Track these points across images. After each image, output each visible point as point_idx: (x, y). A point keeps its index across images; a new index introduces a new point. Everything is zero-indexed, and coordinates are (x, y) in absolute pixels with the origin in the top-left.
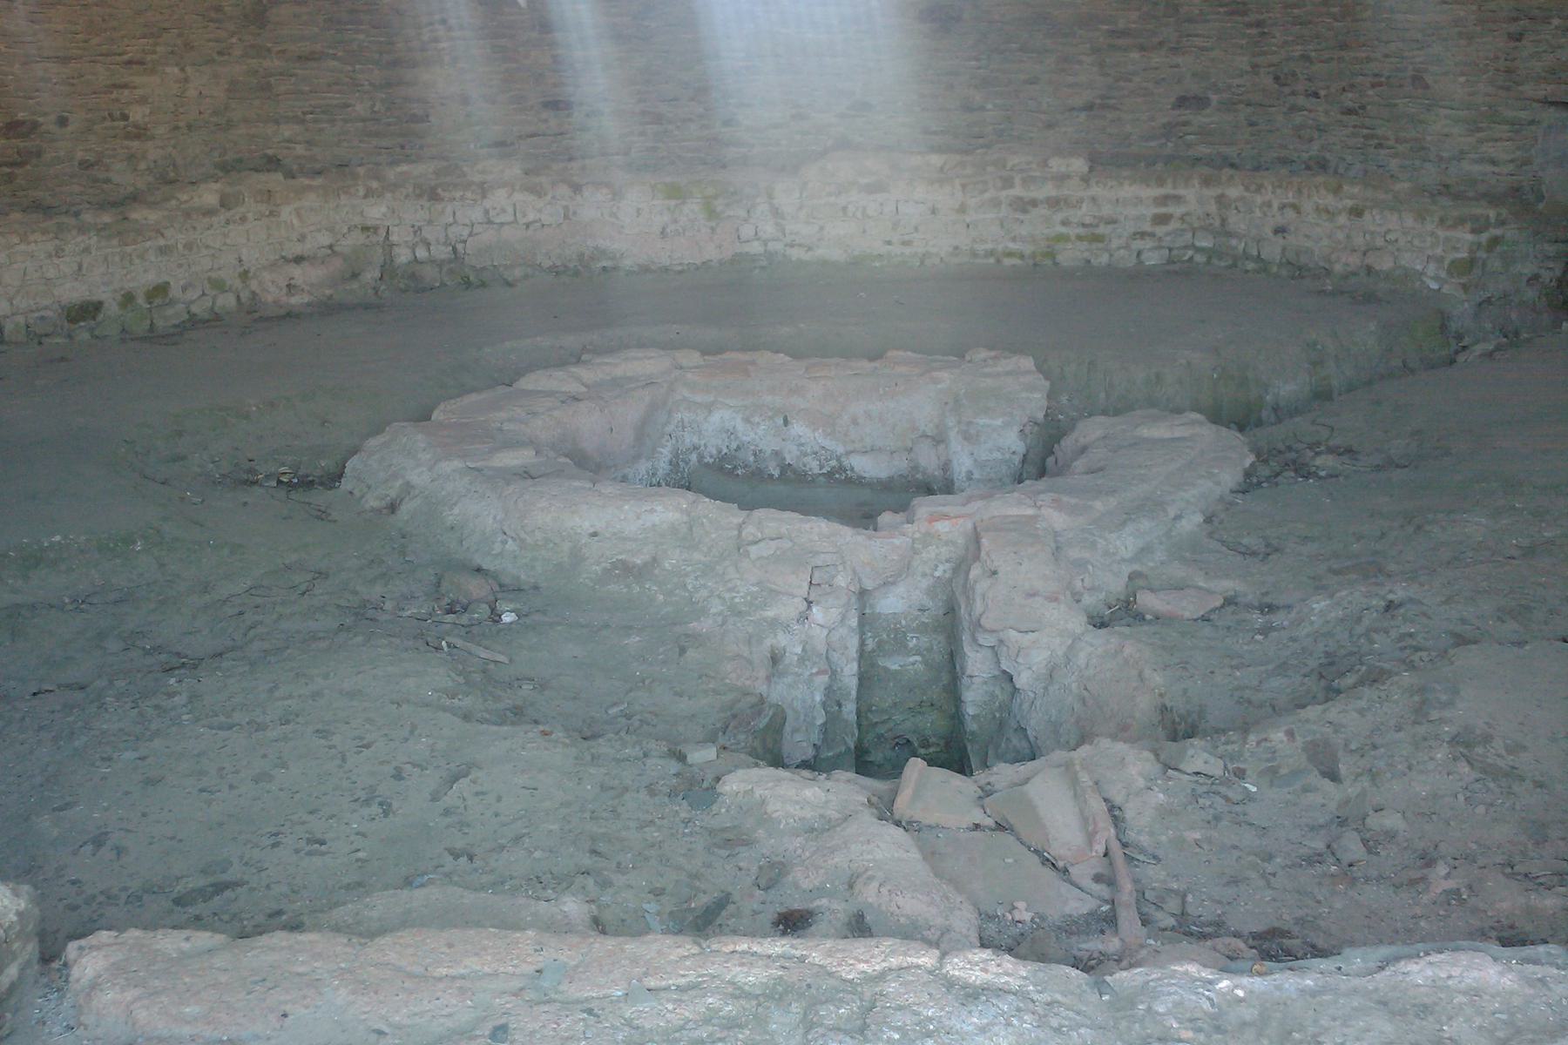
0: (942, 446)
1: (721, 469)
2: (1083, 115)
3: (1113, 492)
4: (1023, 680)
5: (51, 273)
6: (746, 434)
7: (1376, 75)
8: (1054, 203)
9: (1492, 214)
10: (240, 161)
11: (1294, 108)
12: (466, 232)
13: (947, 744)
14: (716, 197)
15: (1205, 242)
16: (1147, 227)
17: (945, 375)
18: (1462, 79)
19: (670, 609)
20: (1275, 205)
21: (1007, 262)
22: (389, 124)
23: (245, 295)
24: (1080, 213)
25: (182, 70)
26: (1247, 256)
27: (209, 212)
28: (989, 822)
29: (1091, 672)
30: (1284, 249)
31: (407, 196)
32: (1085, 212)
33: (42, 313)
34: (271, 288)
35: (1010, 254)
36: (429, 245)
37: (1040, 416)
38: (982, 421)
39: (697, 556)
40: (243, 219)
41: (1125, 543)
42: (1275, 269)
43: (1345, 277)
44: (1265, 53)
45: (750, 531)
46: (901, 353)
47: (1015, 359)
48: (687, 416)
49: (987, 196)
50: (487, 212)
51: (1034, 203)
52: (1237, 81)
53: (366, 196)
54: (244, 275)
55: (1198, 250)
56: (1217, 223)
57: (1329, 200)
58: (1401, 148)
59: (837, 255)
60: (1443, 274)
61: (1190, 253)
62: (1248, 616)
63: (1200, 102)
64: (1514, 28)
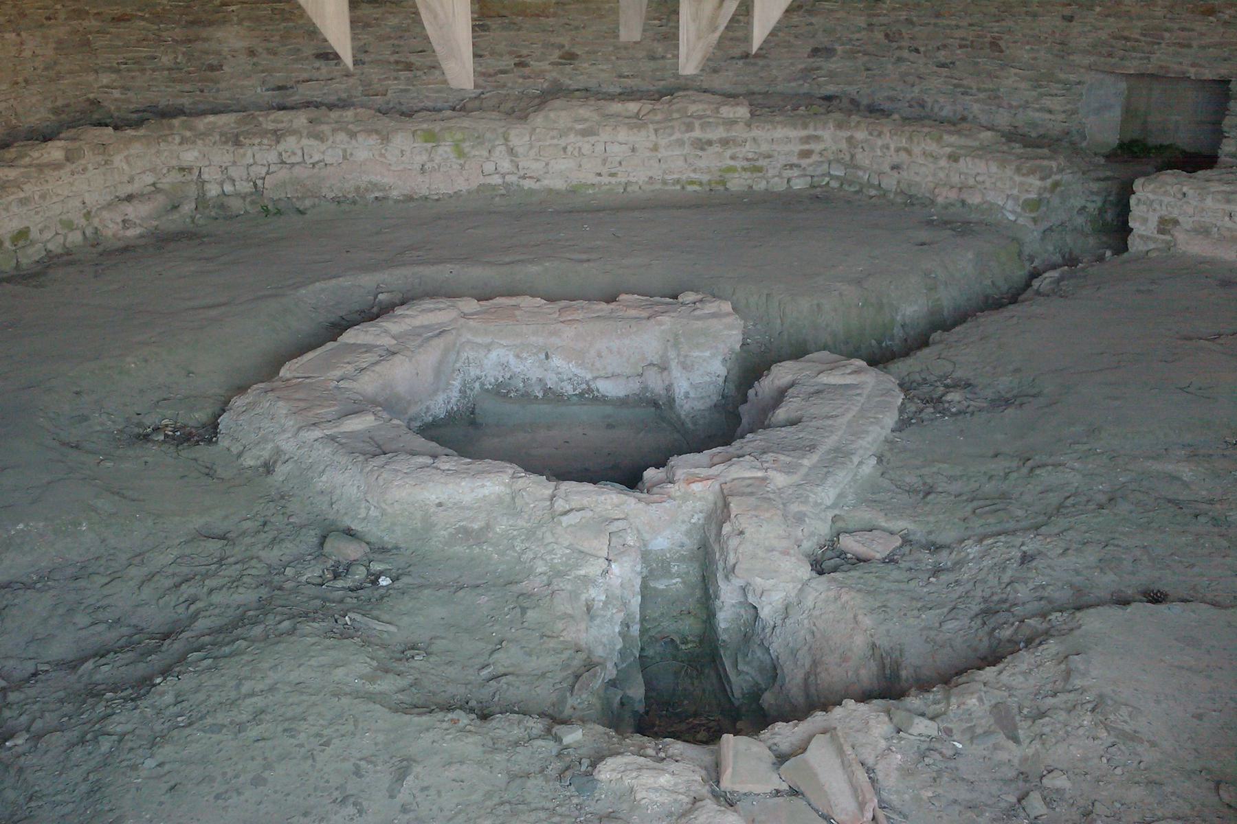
0: (666, 373)
1: (498, 393)
2: (741, 63)
4: (765, 613)
6: (517, 367)
7: (963, 39)
8: (725, 142)
9: (1054, 164)
11: (899, 59)
12: (264, 171)
13: (701, 642)
14: (464, 140)
15: (838, 172)
16: (795, 160)
18: (1028, 47)
19: (504, 567)
20: (892, 147)
21: (690, 188)
23: (89, 232)
24: (744, 150)
25: (19, 35)
27: (57, 166)
28: (784, 787)
29: (817, 613)
30: (899, 182)
31: (215, 143)
32: (748, 150)
34: (111, 226)
35: (692, 183)
37: (737, 347)
38: (696, 354)
39: (521, 523)
41: (827, 494)
42: (892, 196)
43: (945, 207)
45: (560, 505)
47: (716, 303)
48: (472, 354)
50: (280, 154)
51: (710, 143)
52: (856, 36)
53: (181, 144)
54: (88, 215)
55: (832, 177)
56: (848, 158)
57: (932, 147)
58: (982, 96)
59: (560, 184)
60: (1019, 210)
61: (827, 179)
62: (921, 556)
63: (829, 52)
64: (1067, 11)
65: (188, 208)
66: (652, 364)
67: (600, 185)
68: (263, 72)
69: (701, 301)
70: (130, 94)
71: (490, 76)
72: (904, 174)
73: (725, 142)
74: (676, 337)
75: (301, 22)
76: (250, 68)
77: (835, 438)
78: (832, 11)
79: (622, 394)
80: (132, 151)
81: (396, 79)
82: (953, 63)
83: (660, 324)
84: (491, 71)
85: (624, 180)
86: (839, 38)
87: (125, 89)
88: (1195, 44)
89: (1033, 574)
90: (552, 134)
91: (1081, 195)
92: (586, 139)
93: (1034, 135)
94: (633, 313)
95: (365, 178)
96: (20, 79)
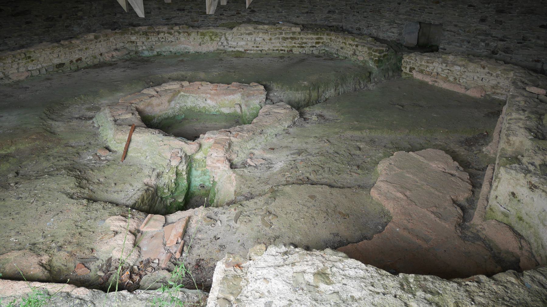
2: (305, 15)
5: (51, 57)
8: (292, 38)
11: (354, 15)
16: (314, 45)
32: (300, 41)
35: (282, 50)
40: (100, 41)
51: (287, 38)
57: (352, 42)
63: (334, 12)
67: (254, 50)
73: (292, 38)
84: (229, 15)
88: (433, 13)
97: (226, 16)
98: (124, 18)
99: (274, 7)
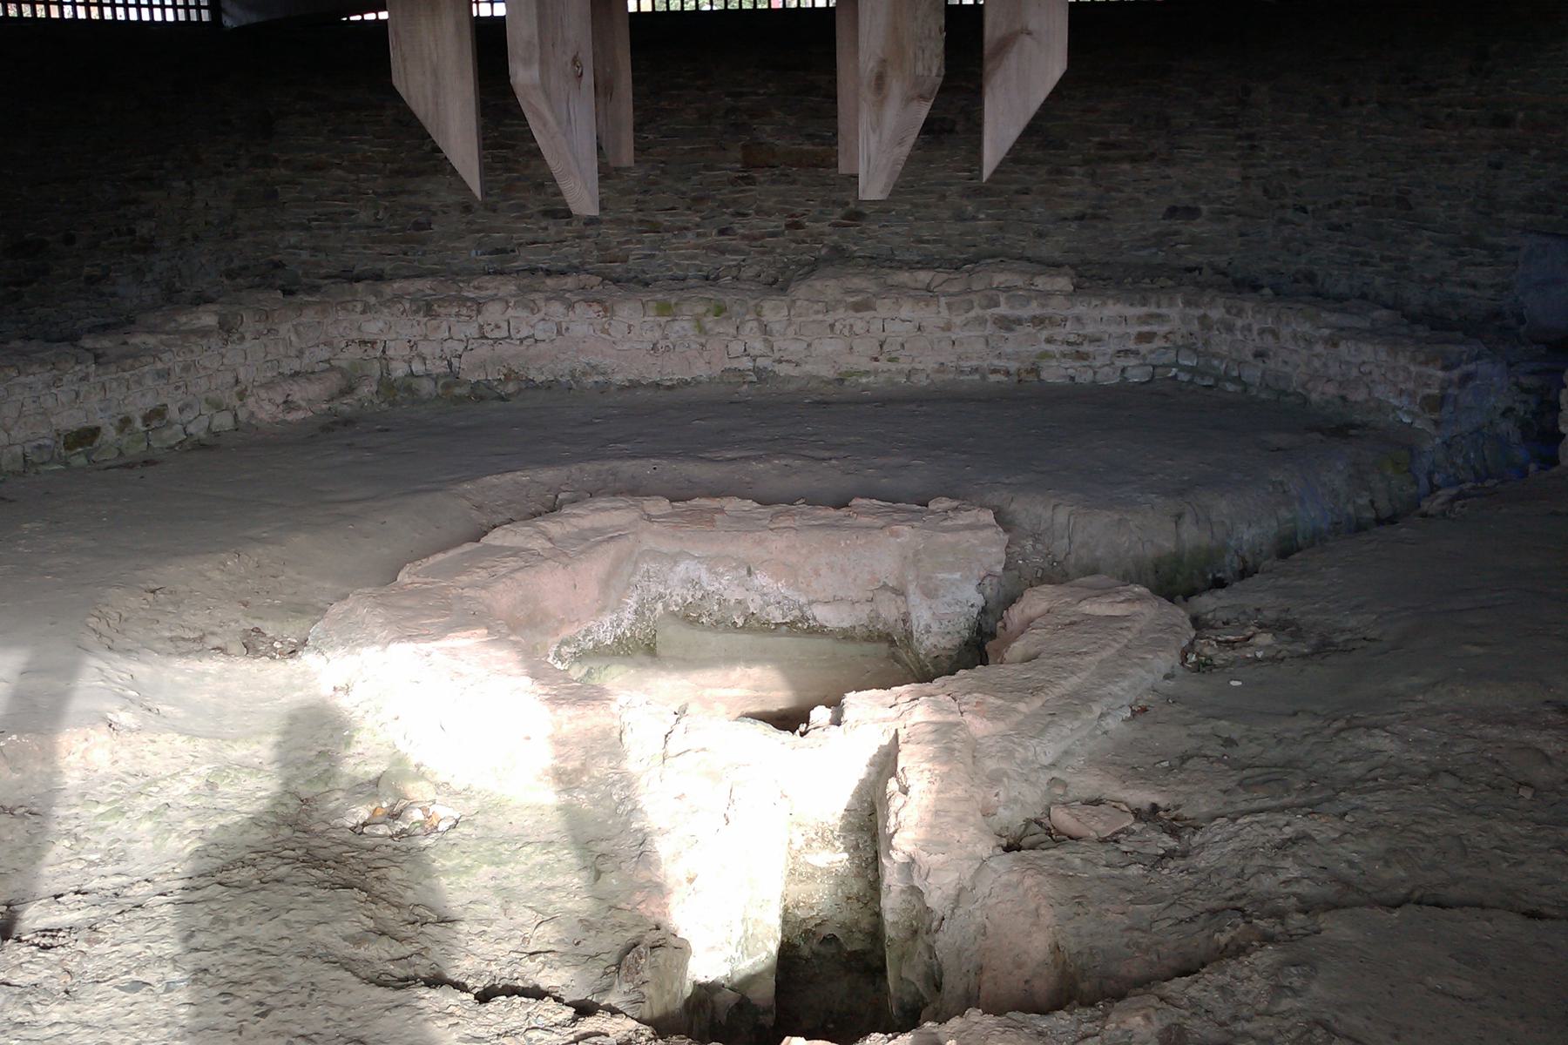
2: (1074, 225)
3: (1036, 690)
5: (50, 402)
8: (1038, 321)
10: (246, 268)
11: (1282, 221)
12: (460, 347)
15: (1189, 361)
16: (1131, 345)
17: (905, 529)
18: (1445, 203)
20: (1255, 327)
21: (993, 378)
22: (392, 231)
25: (189, 183)
26: (1227, 377)
27: (205, 333)
30: (1263, 374)
32: (1068, 331)
33: (41, 442)
34: (264, 409)
35: (995, 371)
36: (424, 359)
44: (1253, 166)
46: (865, 501)
49: (972, 314)
50: (481, 327)
51: (1019, 321)
52: (1226, 193)
55: (1183, 368)
57: (1306, 327)
58: (1386, 267)
59: (827, 372)
60: (1416, 409)
63: (1191, 213)
65: (366, 390)
66: (885, 587)
67: (876, 372)
68: (479, 231)
69: (956, 509)
70: (322, 256)
71: (755, 239)
72: (1271, 364)
73: (1038, 321)
74: (917, 553)
75: (526, 172)
76: (463, 227)
77: (1074, 680)
78: (1195, 160)
79: (846, 625)
80: (303, 319)
81: (639, 242)
82: (1349, 225)
83: (896, 535)
85: (907, 367)
86: (1205, 195)
87: (315, 249)
89: (1288, 863)
90: (816, 307)
91: (1495, 390)
92: (859, 315)
93: (1455, 317)
94: (865, 520)
95: (583, 359)
96: (187, 235)
97: (744, 237)
98: (315, 249)
99: (943, 197)
